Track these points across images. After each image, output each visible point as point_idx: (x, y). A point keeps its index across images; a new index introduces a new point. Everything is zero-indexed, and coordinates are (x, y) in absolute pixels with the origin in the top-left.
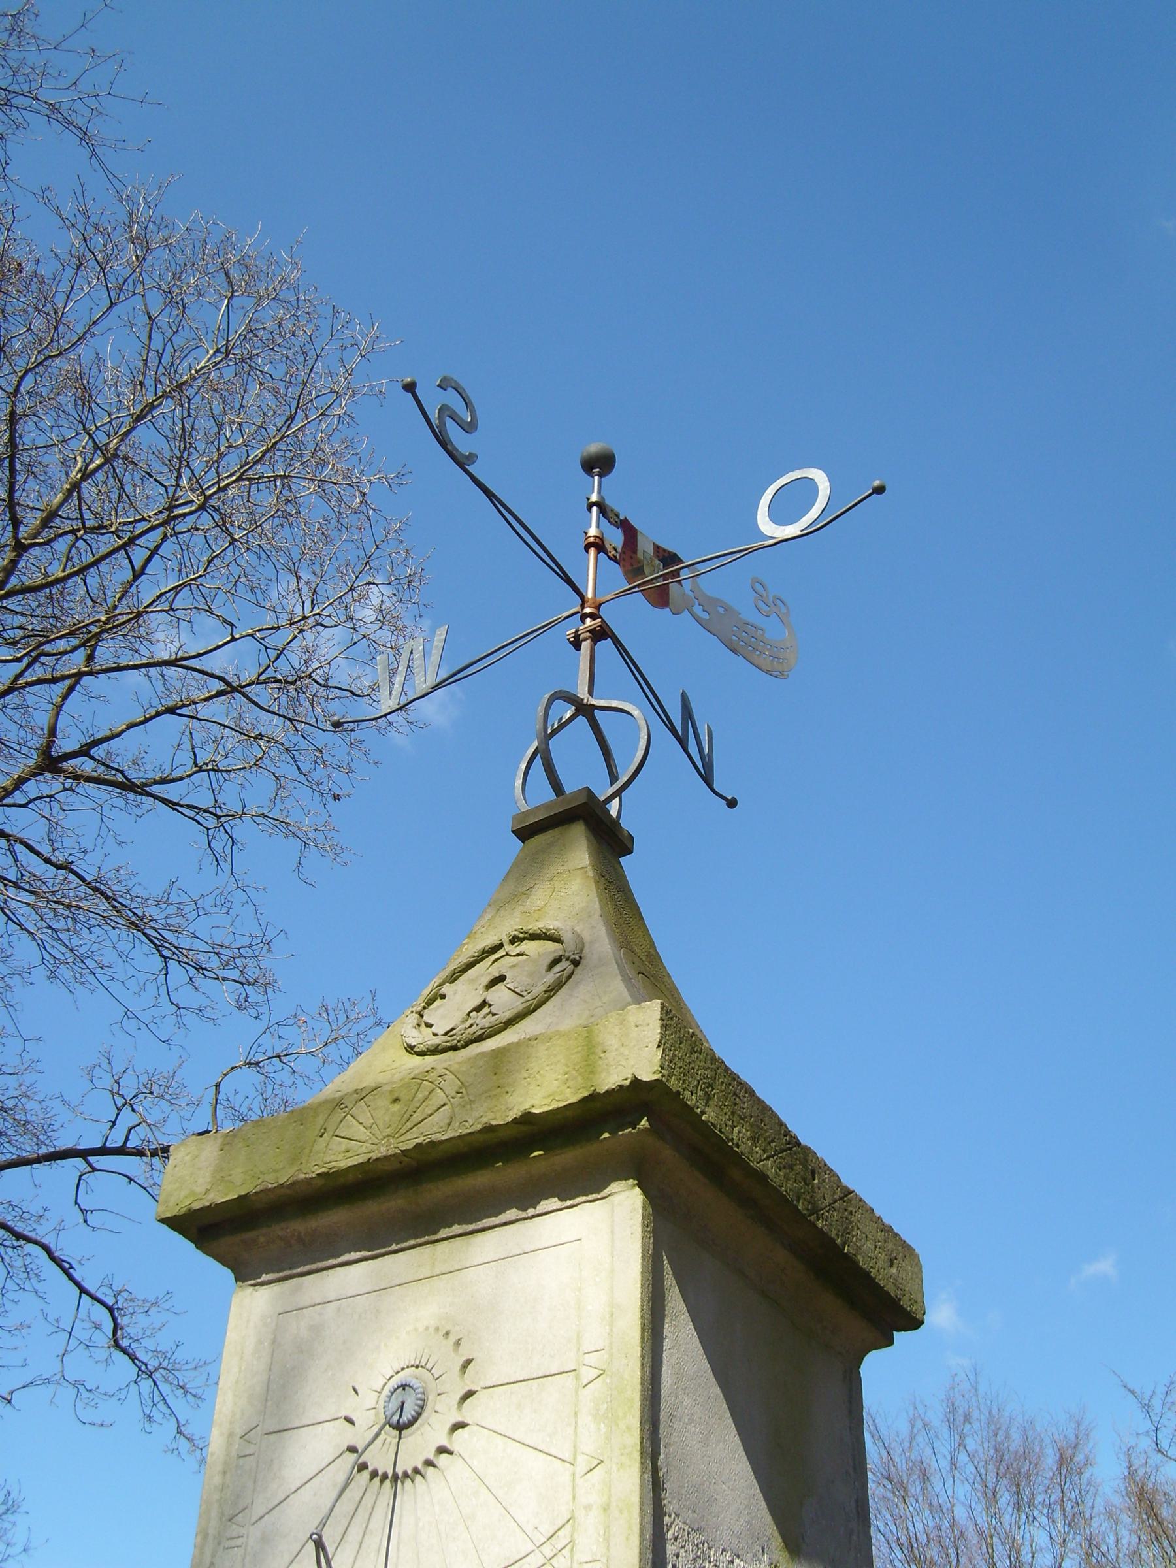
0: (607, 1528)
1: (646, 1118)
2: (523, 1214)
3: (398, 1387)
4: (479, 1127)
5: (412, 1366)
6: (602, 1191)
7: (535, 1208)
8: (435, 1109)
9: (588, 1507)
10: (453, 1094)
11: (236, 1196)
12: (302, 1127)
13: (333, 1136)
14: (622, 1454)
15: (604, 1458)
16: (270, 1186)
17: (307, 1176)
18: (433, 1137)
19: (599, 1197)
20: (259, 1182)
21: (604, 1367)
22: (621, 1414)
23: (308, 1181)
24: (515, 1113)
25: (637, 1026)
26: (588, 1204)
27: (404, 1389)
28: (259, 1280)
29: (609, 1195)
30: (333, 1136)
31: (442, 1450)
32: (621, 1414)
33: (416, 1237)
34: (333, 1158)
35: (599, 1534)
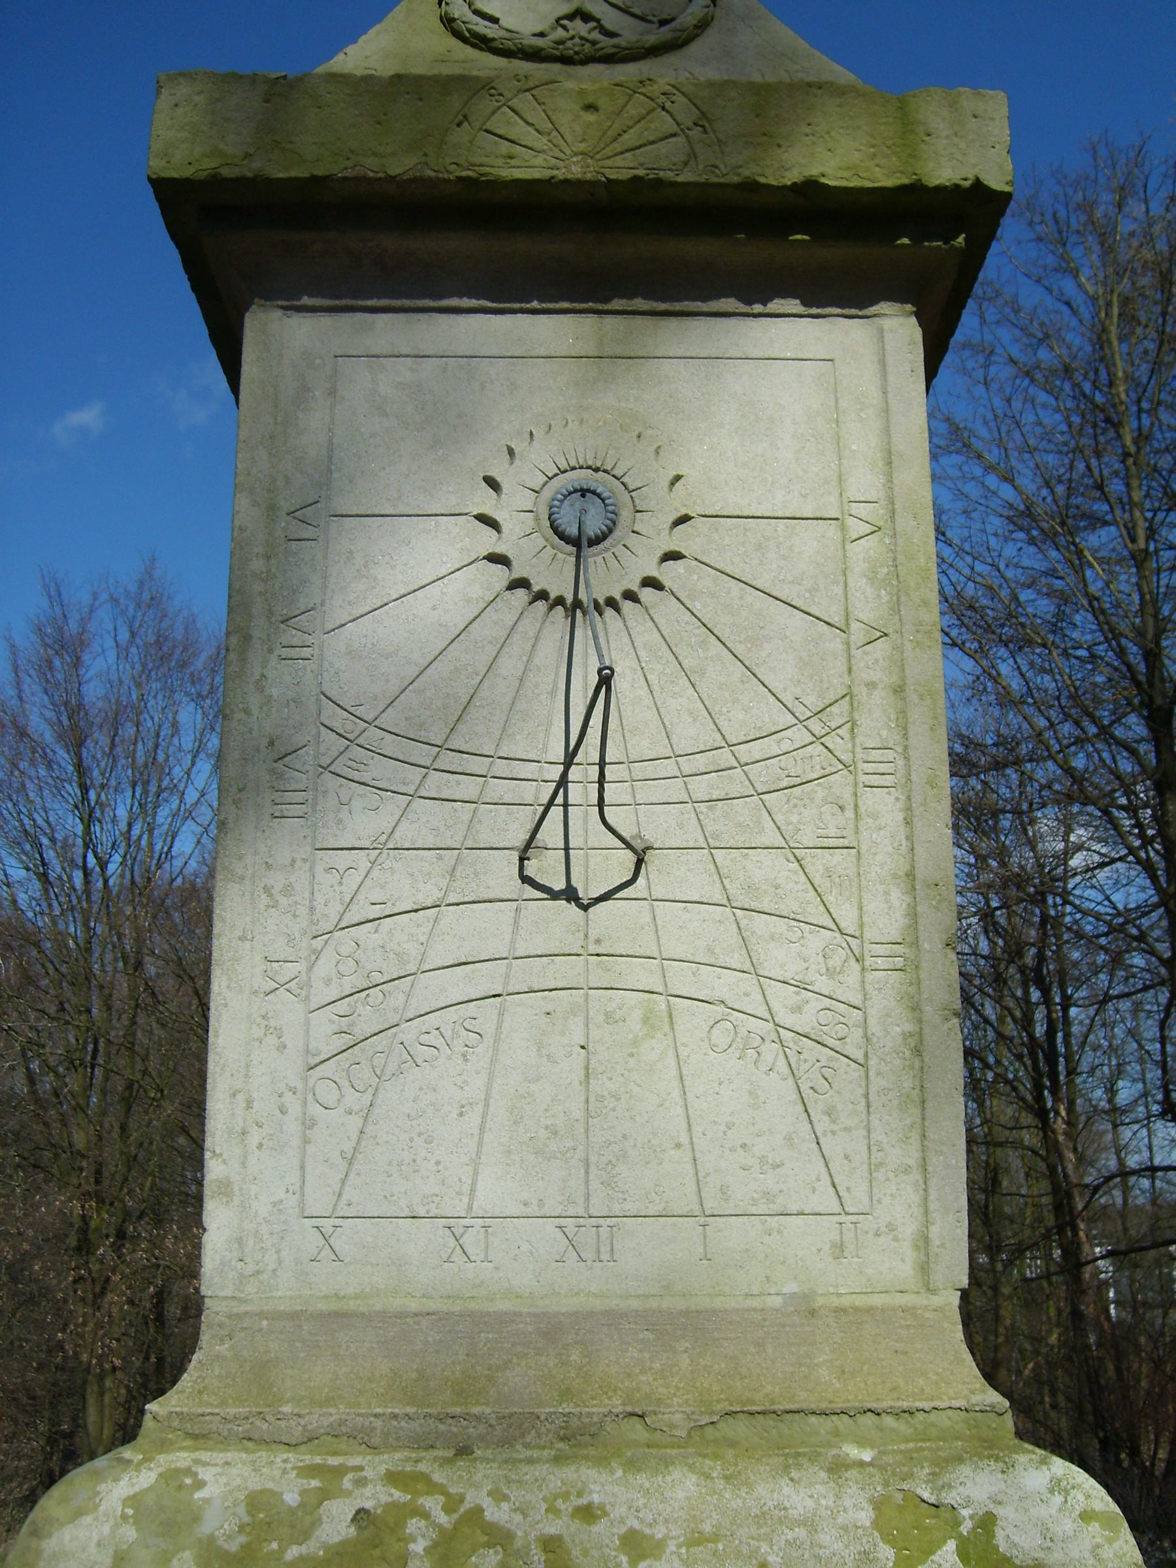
0: (903, 713)
1: (963, 235)
2: (743, 308)
3: (576, 491)
4: (736, 179)
5: (589, 467)
6: (866, 307)
7: (765, 305)
8: (661, 135)
9: (871, 685)
10: (690, 124)
11: (307, 175)
12: (420, 103)
13: (481, 129)
14: (917, 631)
15: (890, 631)
16: (371, 174)
17: (440, 175)
18: (662, 174)
19: (860, 313)
20: (349, 164)
21: (881, 524)
22: (912, 585)
23: (434, 183)
24: (792, 177)
25: (975, 116)
26: (841, 319)
27: (583, 496)
28: (295, 303)
29: (875, 316)
30: (481, 129)
31: (651, 583)
32: (912, 585)
33: (572, 301)
34: (484, 160)
35: (890, 720)
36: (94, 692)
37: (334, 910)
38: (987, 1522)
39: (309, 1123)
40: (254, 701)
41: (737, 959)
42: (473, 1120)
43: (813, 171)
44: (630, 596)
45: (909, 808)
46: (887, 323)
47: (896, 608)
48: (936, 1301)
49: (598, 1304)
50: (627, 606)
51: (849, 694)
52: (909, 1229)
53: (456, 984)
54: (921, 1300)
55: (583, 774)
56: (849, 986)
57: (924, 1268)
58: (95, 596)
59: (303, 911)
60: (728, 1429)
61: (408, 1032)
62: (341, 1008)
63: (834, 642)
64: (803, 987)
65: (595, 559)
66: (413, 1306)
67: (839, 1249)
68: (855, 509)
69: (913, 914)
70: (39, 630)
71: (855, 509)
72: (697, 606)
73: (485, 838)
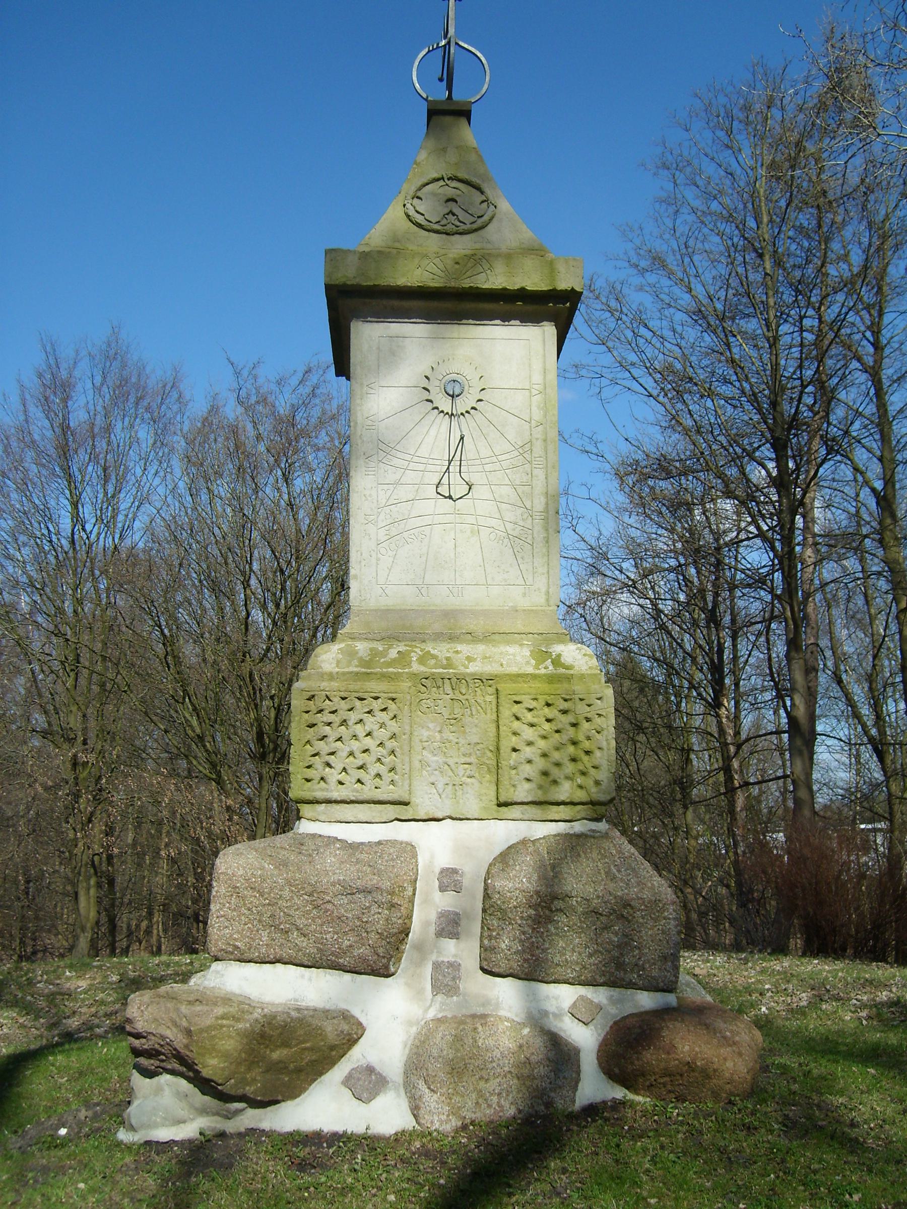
9: (537, 439)
31: (473, 408)
36: (78, 417)
37: (384, 501)
38: (559, 656)
39: (378, 559)
40: (359, 442)
41: (497, 516)
42: (424, 558)
43: (523, 285)
44: (467, 412)
45: (547, 474)
46: (546, 328)
47: (545, 416)
48: (551, 608)
49: (458, 608)
50: (467, 415)
51: (531, 441)
52: (544, 590)
53: (418, 522)
54: (547, 608)
55: (456, 463)
56: (528, 524)
57: (548, 600)
58: (77, 352)
59: (375, 501)
60: (493, 637)
61: (405, 535)
62: (387, 528)
63: (527, 426)
64: (515, 524)
65: (458, 400)
66: (408, 608)
67: (524, 595)
68: (534, 386)
69: (547, 504)
70: (40, 376)
71: (534, 386)
72: (487, 415)
73: (426, 481)
